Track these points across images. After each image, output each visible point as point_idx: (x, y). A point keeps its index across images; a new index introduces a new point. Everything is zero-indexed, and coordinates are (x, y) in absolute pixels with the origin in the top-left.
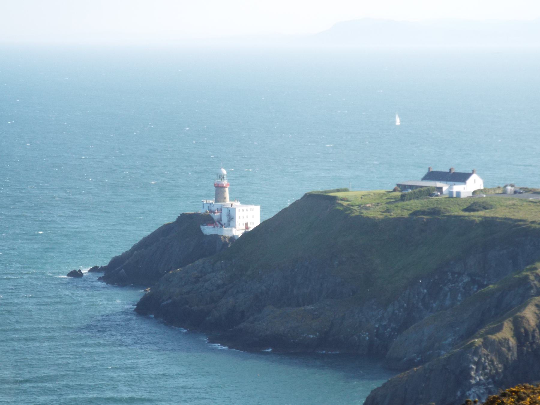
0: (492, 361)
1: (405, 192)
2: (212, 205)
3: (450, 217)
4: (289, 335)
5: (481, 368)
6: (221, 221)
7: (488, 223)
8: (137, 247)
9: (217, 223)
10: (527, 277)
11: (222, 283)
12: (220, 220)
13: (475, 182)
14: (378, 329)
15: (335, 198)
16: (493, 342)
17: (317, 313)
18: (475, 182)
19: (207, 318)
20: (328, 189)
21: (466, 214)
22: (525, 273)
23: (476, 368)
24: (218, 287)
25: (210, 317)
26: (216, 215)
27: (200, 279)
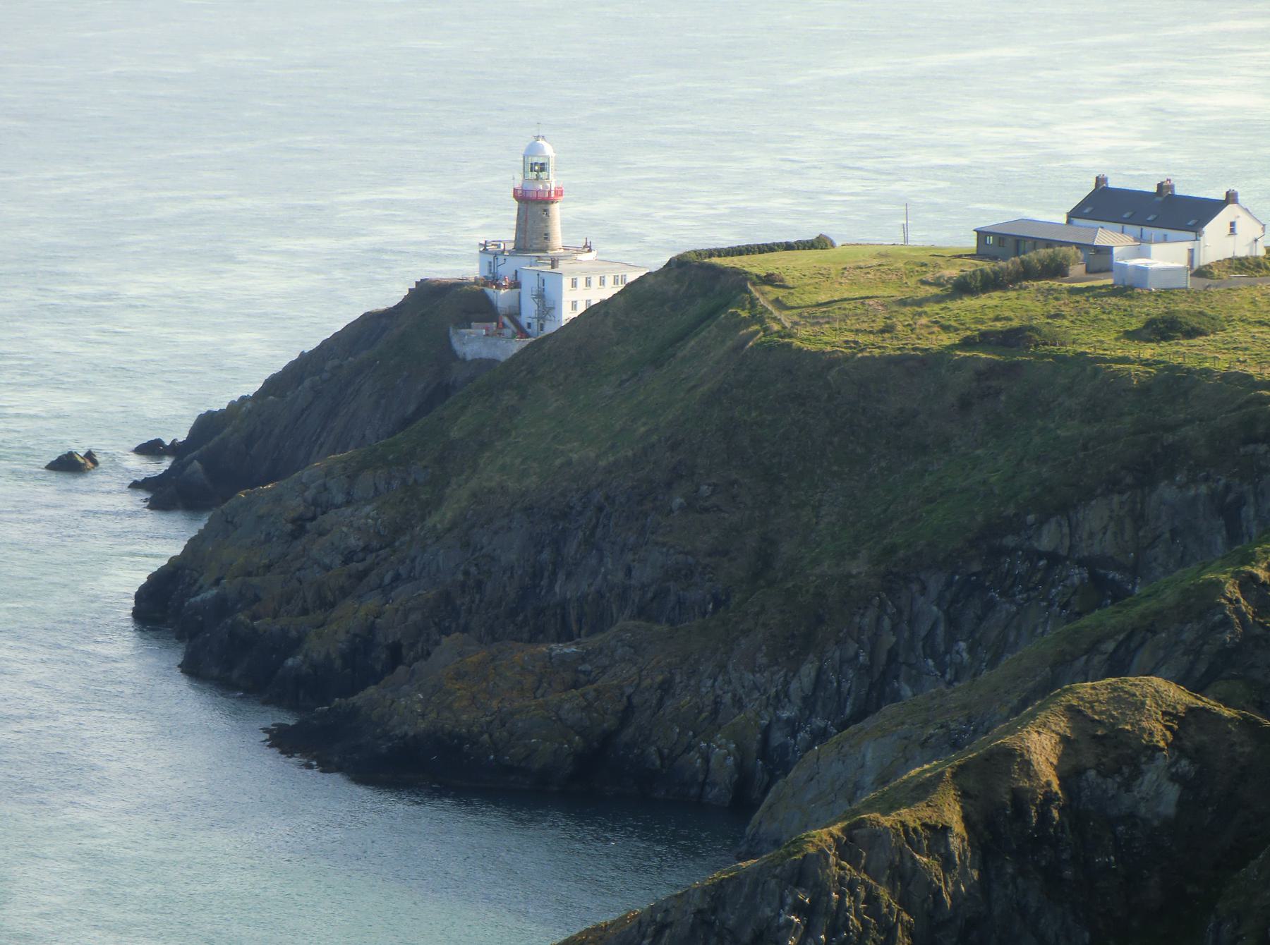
0: (872, 899)
1: (1011, 256)
2: (501, 259)
3: (1062, 359)
4: (486, 736)
5: (823, 922)
6: (520, 314)
7: (1175, 384)
8: (274, 385)
9: (506, 320)
10: (1217, 586)
11: (361, 544)
12: (514, 315)
13: (1232, 231)
14: (766, 731)
15: (740, 280)
16: (877, 837)
17: (587, 667)
18: (1232, 231)
19: (290, 662)
20: (735, 244)
21: (1149, 351)
22: (1222, 577)
23: (807, 927)
24: (349, 557)
25: (300, 658)
26: (501, 297)
27: (308, 526)
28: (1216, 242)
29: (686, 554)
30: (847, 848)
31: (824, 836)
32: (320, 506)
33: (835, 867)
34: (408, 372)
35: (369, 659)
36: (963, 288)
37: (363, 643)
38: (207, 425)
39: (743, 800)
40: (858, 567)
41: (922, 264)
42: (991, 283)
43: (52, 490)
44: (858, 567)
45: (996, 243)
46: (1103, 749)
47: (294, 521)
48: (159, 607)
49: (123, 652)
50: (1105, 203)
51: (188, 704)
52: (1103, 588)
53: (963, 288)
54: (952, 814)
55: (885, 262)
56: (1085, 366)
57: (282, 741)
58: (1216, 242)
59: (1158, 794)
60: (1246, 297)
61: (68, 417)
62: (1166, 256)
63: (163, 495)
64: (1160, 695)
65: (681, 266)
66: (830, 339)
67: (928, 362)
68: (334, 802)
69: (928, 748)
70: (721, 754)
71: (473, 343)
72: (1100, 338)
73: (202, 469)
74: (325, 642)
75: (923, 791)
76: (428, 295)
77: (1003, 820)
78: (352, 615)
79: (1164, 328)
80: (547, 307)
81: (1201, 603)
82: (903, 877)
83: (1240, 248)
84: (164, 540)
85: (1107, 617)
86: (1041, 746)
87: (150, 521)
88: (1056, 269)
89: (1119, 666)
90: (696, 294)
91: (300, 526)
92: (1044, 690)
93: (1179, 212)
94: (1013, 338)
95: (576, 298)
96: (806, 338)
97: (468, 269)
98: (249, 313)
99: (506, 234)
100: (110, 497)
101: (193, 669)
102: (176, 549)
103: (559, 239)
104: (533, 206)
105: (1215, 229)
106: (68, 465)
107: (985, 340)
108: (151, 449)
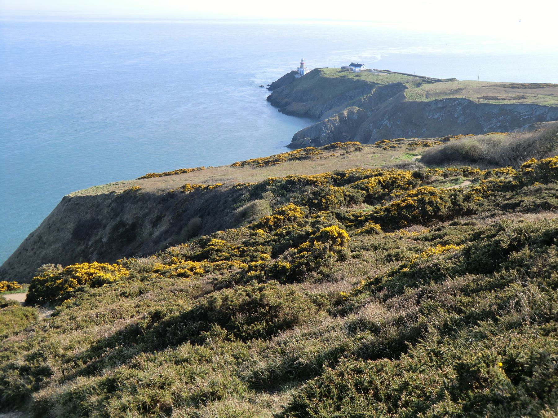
1: (344, 69)
7: (358, 81)
15: (320, 71)
16: (331, 120)
26: (299, 72)
28: (362, 68)
29: (463, 242)
30: (328, 121)
31: (326, 120)
32: (283, 90)
33: (327, 123)
34: (290, 79)
35: (287, 104)
36: (340, 72)
37: (286, 103)
38: (273, 83)
39: (319, 117)
40: (330, 96)
41: (336, 69)
42: (342, 71)
43: (260, 89)
44: (330, 96)
45: (343, 68)
46: (351, 113)
47: (46, 358)
48: (269, 99)
49: (266, 102)
50: (352, 65)
51: (272, 108)
52: (351, 98)
53: (340, 72)
54: (337, 118)
55: (333, 69)
56: (350, 79)
57: (279, 111)
58: (362, 68)
59: (355, 117)
60: (365, 73)
61: (259, 82)
62: (358, 69)
63: (269, 89)
64: (356, 108)
65: (315, 70)
66: (328, 76)
67: (336, 79)
68: (284, 116)
69: (336, 113)
70: (318, 113)
71: (297, 76)
72: (351, 76)
73: (273, 87)
74: (284, 102)
75: (335, 116)
76: (293, 72)
77: (342, 119)
78: (286, 100)
79: (357, 76)
80: (303, 73)
81: (360, 100)
82: (333, 124)
83: (364, 69)
84: (269, 93)
85: (352, 101)
86: (345, 112)
87: (268, 91)
88: (348, 70)
89: (352, 106)
90: (316, 72)
91: (281, 92)
92: (346, 107)
93: (359, 66)
94: (344, 77)
95: (305, 73)
96: (326, 76)
97: (296, 70)
98: (277, 73)
99: (300, 66)
100: (265, 89)
101: (272, 105)
102: (270, 94)
103: (304, 67)
104: (302, 64)
105: (362, 67)
106: (261, 87)
107: (342, 77)
108: (268, 85)
